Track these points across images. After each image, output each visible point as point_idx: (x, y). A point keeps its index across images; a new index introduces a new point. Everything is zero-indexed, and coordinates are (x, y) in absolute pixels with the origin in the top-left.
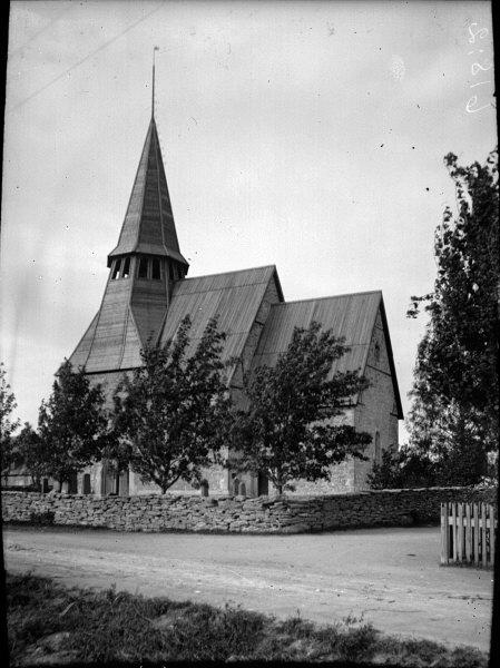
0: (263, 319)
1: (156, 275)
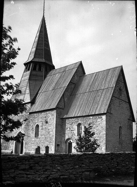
0: (75, 81)
1: (40, 70)
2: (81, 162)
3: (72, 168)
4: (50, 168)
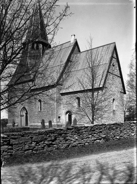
2: (94, 132)
3: (87, 138)
4: (70, 139)
